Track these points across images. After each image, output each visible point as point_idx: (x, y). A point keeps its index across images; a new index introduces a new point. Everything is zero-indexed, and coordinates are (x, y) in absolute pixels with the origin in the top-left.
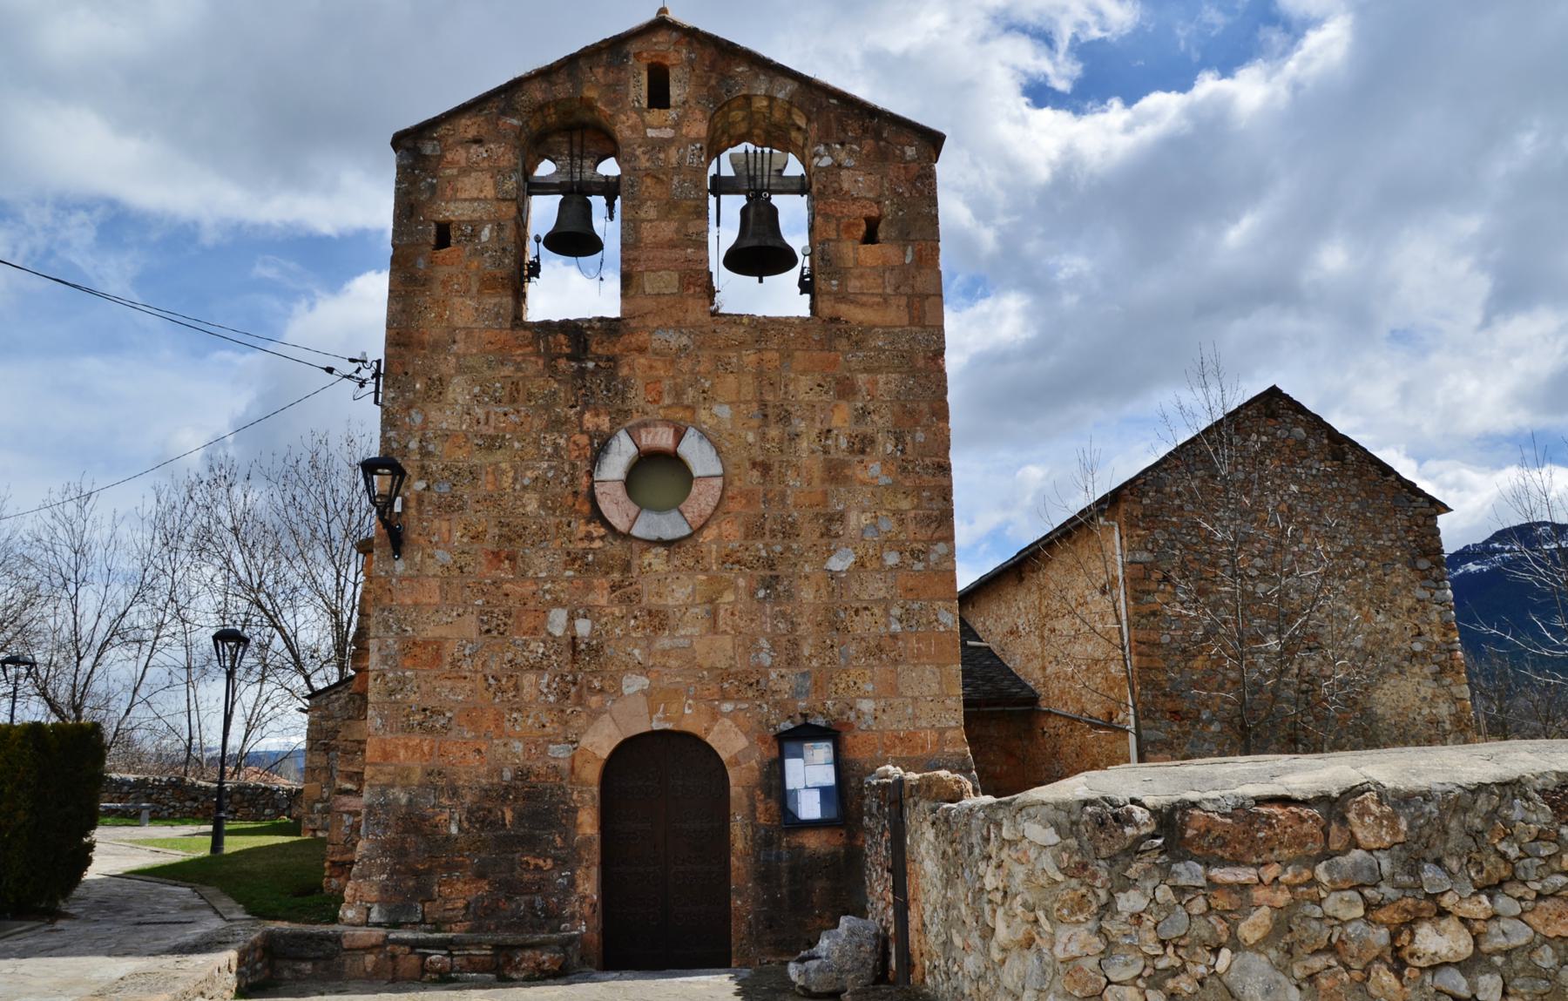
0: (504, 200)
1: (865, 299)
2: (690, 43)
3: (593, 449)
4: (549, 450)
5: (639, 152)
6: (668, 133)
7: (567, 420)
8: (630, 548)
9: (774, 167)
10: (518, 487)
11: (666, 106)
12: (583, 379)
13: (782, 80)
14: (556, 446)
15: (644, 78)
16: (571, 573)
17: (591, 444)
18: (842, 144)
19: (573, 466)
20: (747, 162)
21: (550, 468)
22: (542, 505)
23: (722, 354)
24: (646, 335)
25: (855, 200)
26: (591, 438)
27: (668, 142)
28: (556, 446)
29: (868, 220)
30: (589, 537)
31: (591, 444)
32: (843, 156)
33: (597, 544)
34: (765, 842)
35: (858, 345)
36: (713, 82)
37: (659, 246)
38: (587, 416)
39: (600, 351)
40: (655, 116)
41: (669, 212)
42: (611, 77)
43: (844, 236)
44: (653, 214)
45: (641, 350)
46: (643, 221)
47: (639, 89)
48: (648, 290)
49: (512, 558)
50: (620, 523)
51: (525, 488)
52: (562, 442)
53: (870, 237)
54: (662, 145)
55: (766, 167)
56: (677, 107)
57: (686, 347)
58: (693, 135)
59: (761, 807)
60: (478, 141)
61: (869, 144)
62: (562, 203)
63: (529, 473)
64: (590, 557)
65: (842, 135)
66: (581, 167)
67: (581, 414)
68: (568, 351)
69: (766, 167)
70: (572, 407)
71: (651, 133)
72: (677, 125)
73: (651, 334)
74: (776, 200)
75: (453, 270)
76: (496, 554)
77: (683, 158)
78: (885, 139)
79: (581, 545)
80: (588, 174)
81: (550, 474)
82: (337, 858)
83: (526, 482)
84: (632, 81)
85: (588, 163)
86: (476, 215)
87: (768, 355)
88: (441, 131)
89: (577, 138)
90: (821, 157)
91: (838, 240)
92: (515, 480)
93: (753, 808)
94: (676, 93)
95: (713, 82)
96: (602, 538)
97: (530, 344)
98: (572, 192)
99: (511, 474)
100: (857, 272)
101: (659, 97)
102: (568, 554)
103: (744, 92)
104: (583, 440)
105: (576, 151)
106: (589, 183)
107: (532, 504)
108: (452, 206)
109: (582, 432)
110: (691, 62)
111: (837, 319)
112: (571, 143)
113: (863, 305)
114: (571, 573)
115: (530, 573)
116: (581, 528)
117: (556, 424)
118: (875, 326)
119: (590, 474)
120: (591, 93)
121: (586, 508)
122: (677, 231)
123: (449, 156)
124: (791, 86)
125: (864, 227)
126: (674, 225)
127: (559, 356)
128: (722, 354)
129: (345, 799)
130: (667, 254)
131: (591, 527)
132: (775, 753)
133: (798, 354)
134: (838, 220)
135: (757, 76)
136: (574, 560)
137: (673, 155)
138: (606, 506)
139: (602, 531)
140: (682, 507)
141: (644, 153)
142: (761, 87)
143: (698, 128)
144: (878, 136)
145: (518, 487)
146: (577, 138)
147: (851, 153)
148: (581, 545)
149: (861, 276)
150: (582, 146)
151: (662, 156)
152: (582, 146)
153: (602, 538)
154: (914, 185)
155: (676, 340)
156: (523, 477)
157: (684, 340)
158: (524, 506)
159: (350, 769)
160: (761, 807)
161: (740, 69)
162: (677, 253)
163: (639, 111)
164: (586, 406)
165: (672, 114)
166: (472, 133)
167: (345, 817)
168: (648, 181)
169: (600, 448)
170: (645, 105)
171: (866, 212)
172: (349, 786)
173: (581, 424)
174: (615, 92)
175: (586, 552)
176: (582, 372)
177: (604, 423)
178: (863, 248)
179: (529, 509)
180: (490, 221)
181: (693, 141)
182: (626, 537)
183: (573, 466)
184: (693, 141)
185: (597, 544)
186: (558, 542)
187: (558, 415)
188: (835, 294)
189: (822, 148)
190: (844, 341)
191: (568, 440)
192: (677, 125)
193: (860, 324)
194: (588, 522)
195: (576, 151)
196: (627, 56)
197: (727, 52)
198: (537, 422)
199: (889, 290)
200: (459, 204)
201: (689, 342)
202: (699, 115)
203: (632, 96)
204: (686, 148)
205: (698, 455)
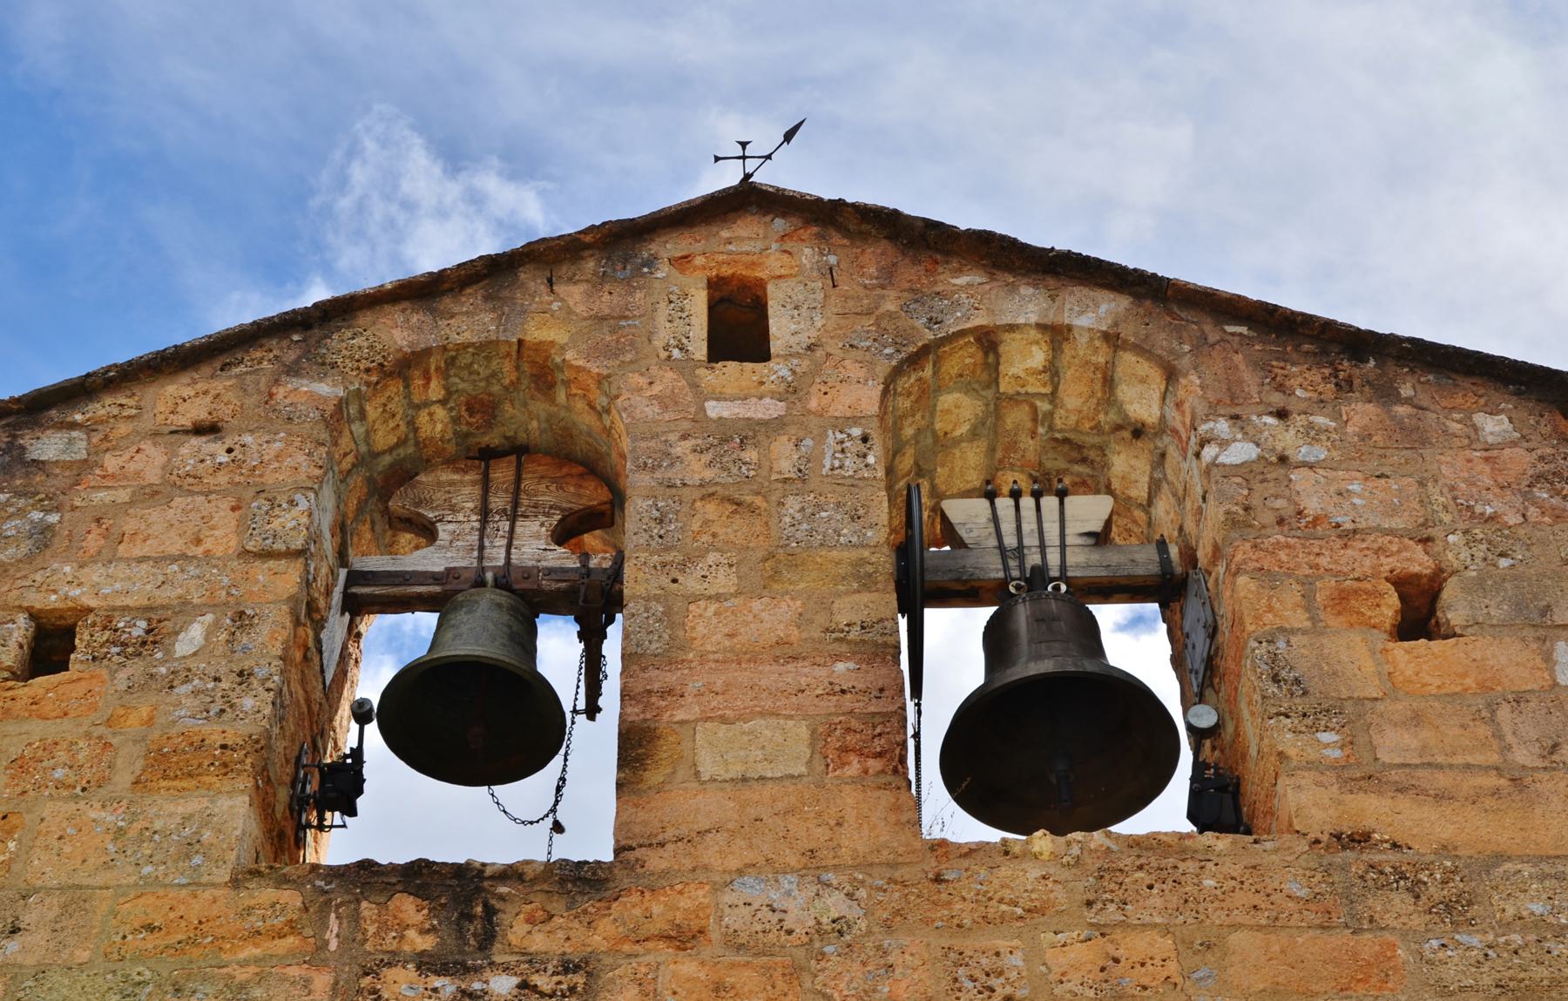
0: (267, 555)
1: (1443, 780)
6: (770, 409)
11: (763, 355)
18: (1282, 414)
23: (968, 944)
24: (701, 895)
25: (1348, 536)
27: (774, 426)
29: (1402, 583)
35: (1456, 910)
36: (890, 306)
37: (748, 656)
39: (539, 942)
41: (775, 575)
42: (607, 301)
43: (1334, 622)
44: (724, 581)
45: (683, 938)
46: (694, 599)
48: (708, 768)
53: (1419, 616)
54: (750, 433)
57: (840, 927)
58: (839, 409)
60: (207, 429)
65: (1277, 399)
68: (426, 943)
71: (714, 409)
73: (717, 888)
75: (51, 729)
84: (663, 311)
86: (169, 594)
87: (1134, 945)
88: (102, 408)
90: (1224, 444)
91: (1317, 628)
97: (292, 927)
100: (1399, 708)
105: (498, 501)
108: (95, 574)
111: (1360, 839)
112: (486, 485)
113: (1440, 797)
118: (1500, 857)
122: (802, 620)
123: (111, 463)
125: (1393, 600)
126: (788, 608)
127: (393, 959)
128: (968, 944)
130: (770, 675)
133: (1236, 939)
134: (1307, 583)
137: (784, 456)
149: (1417, 719)
154: (1527, 496)
155: (801, 905)
157: (836, 905)
162: (804, 674)
163: (686, 367)
166: (198, 411)
168: (711, 509)
170: (700, 350)
171: (1388, 563)
178: (1400, 650)
180: (213, 606)
188: (1338, 768)
189: (1222, 427)
190: (1400, 901)
193: (1445, 849)
195: (498, 501)
196: (651, 262)
199: (1523, 756)
200: (120, 570)
201: (852, 912)
204: (823, 436)
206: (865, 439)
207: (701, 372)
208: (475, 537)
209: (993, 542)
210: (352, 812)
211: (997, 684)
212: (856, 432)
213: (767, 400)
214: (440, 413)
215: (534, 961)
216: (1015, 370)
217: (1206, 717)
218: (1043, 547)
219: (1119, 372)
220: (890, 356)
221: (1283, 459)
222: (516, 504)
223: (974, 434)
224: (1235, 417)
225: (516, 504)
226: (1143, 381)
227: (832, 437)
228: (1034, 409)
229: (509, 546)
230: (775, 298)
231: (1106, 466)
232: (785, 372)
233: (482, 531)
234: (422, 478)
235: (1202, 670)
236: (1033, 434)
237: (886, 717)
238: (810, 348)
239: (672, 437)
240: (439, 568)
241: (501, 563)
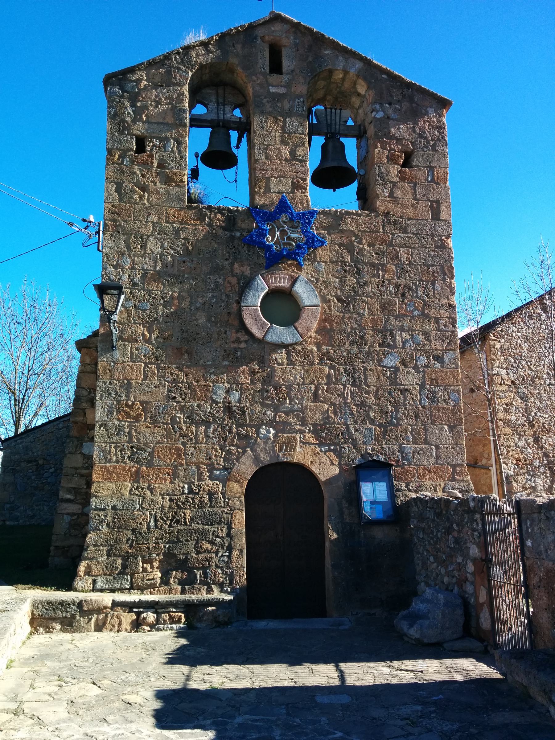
2: (295, 33)
3: (240, 287)
4: (212, 286)
5: (265, 101)
6: (282, 90)
7: (224, 267)
8: (263, 349)
9: (343, 120)
10: (193, 308)
12: (233, 242)
13: (352, 60)
14: (217, 284)
15: (267, 54)
16: (227, 363)
17: (239, 283)
18: (390, 104)
19: (228, 296)
20: (326, 115)
21: (213, 297)
22: (209, 320)
26: (239, 280)
28: (217, 284)
30: (238, 341)
31: (239, 283)
32: (390, 112)
33: (243, 345)
34: (347, 533)
36: (310, 59)
38: (236, 266)
39: (243, 226)
40: (274, 78)
47: (264, 60)
49: (189, 353)
50: (258, 333)
51: (197, 309)
52: (221, 281)
55: (338, 118)
56: (287, 74)
59: (346, 512)
61: (406, 105)
62: (212, 134)
63: (200, 300)
64: (239, 353)
66: (224, 111)
67: (232, 265)
69: (338, 118)
70: (226, 260)
71: (272, 90)
72: (288, 86)
74: (342, 140)
76: (179, 350)
77: (292, 107)
78: (416, 103)
79: (233, 346)
80: (228, 116)
81: (213, 301)
82: (59, 544)
83: (198, 305)
84: (260, 55)
85: (228, 108)
89: (221, 91)
90: (377, 112)
92: (191, 304)
93: (341, 513)
94: (286, 64)
95: (310, 59)
96: (246, 342)
98: (218, 126)
99: (189, 300)
101: (276, 67)
102: (225, 351)
103: (330, 67)
104: (234, 281)
105: (221, 100)
106: (229, 121)
107: (202, 320)
109: (233, 276)
110: (296, 45)
114: (227, 363)
115: (201, 362)
116: (234, 336)
117: (217, 270)
119: (238, 303)
120: (234, 60)
121: (236, 323)
124: (359, 65)
129: (65, 505)
131: (239, 335)
132: (353, 477)
135: (337, 57)
136: (228, 355)
138: (249, 322)
139: (246, 337)
140: (297, 324)
141: (268, 102)
142: (340, 63)
143: (301, 89)
144: (411, 99)
145: (193, 308)
146: (221, 91)
147: (396, 110)
148: (233, 346)
150: (224, 97)
151: (279, 105)
152: (224, 97)
153: (246, 342)
156: (196, 302)
158: (197, 320)
159: (70, 485)
160: (346, 512)
161: (326, 52)
164: (235, 259)
165: (285, 78)
167: (65, 516)
169: (246, 284)
170: (268, 71)
172: (68, 496)
173: (232, 271)
174: (249, 64)
175: (236, 350)
176: (233, 237)
177: (247, 270)
179: (200, 322)
181: (299, 97)
182: (261, 342)
183: (228, 296)
184: (299, 97)
185: (243, 345)
186: (219, 343)
187: (218, 264)
189: (378, 106)
191: (224, 280)
192: (288, 86)
194: (237, 332)
196: (256, 38)
197: (319, 40)
198: (204, 268)
202: (302, 80)
203: (260, 64)
204: (294, 101)
205: (305, 293)
206: (303, 102)
207: (268, 77)
208: (216, 110)
209: (325, 122)
210: (197, 179)
211: (325, 167)
212: (302, 100)
213: (283, 88)
214: (207, 75)
215: (243, 229)
216: (336, 77)
217: (362, 172)
218: (335, 124)
219: (358, 82)
220: (309, 76)
221: (388, 118)
222: (224, 101)
223: (323, 88)
224: (381, 104)
225: (224, 101)
226: (363, 86)
227: (297, 101)
228: (337, 85)
229: (224, 114)
230: (284, 53)
231: (350, 99)
232: (286, 79)
233: (218, 108)
234: (203, 91)
235: (363, 160)
236: (336, 90)
237: (416, 503)
238: (292, 71)
239: (263, 98)
240: (209, 119)
241: (222, 118)
